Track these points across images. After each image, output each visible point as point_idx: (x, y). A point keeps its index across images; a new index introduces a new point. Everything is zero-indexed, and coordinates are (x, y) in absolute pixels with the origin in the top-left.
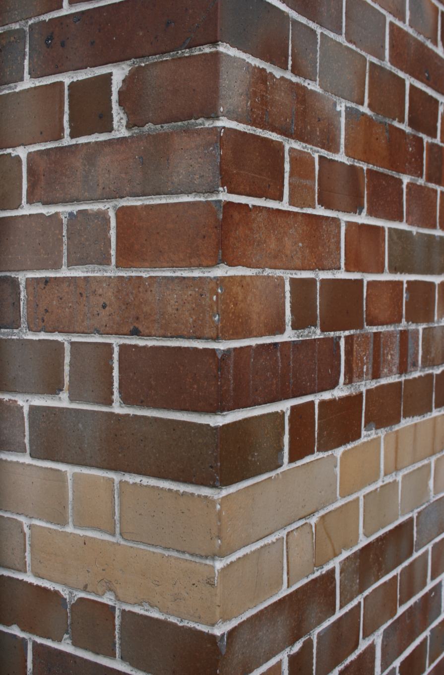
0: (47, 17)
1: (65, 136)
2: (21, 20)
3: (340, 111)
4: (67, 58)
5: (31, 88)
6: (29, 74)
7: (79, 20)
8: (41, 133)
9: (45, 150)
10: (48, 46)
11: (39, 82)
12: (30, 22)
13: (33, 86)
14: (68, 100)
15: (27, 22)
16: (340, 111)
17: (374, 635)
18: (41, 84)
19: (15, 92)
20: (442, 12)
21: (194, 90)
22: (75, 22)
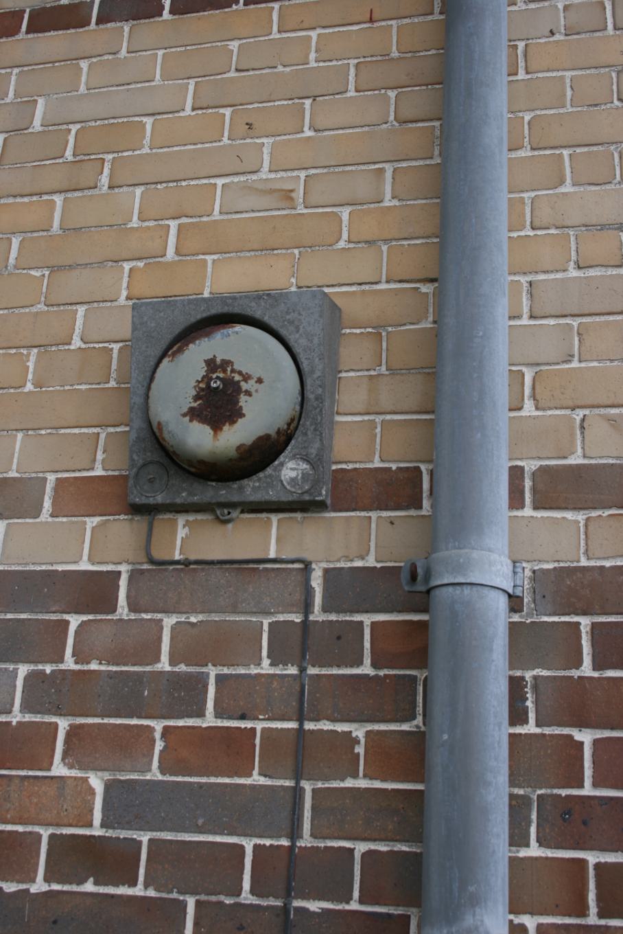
0: (564, 792)
1: (591, 915)
2: (527, 787)
3: (358, 754)
4: (591, 837)
5: (541, 858)
6: (538, 841)
7: (606, 804)
8: (557, 906)
9: (561, 924)
10: (564, 820)
11: (552, 853)
12: (539, 792)
13: (543, 855)
14: (594, 879)
15: (535, 791)
16: (358, 754)
17: (424, 285)
18: (555, 855)
19: (518, 857)
20: (28, 890)
21: (53, 376)
22: (601, 805)
